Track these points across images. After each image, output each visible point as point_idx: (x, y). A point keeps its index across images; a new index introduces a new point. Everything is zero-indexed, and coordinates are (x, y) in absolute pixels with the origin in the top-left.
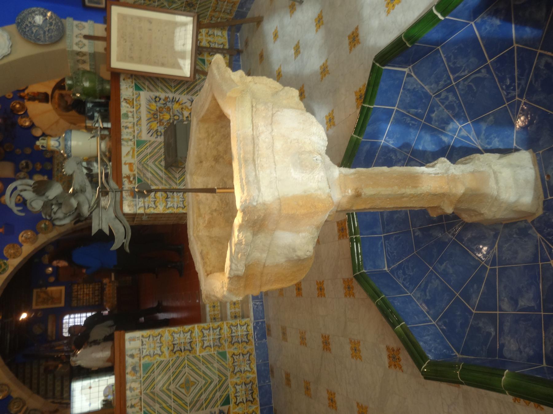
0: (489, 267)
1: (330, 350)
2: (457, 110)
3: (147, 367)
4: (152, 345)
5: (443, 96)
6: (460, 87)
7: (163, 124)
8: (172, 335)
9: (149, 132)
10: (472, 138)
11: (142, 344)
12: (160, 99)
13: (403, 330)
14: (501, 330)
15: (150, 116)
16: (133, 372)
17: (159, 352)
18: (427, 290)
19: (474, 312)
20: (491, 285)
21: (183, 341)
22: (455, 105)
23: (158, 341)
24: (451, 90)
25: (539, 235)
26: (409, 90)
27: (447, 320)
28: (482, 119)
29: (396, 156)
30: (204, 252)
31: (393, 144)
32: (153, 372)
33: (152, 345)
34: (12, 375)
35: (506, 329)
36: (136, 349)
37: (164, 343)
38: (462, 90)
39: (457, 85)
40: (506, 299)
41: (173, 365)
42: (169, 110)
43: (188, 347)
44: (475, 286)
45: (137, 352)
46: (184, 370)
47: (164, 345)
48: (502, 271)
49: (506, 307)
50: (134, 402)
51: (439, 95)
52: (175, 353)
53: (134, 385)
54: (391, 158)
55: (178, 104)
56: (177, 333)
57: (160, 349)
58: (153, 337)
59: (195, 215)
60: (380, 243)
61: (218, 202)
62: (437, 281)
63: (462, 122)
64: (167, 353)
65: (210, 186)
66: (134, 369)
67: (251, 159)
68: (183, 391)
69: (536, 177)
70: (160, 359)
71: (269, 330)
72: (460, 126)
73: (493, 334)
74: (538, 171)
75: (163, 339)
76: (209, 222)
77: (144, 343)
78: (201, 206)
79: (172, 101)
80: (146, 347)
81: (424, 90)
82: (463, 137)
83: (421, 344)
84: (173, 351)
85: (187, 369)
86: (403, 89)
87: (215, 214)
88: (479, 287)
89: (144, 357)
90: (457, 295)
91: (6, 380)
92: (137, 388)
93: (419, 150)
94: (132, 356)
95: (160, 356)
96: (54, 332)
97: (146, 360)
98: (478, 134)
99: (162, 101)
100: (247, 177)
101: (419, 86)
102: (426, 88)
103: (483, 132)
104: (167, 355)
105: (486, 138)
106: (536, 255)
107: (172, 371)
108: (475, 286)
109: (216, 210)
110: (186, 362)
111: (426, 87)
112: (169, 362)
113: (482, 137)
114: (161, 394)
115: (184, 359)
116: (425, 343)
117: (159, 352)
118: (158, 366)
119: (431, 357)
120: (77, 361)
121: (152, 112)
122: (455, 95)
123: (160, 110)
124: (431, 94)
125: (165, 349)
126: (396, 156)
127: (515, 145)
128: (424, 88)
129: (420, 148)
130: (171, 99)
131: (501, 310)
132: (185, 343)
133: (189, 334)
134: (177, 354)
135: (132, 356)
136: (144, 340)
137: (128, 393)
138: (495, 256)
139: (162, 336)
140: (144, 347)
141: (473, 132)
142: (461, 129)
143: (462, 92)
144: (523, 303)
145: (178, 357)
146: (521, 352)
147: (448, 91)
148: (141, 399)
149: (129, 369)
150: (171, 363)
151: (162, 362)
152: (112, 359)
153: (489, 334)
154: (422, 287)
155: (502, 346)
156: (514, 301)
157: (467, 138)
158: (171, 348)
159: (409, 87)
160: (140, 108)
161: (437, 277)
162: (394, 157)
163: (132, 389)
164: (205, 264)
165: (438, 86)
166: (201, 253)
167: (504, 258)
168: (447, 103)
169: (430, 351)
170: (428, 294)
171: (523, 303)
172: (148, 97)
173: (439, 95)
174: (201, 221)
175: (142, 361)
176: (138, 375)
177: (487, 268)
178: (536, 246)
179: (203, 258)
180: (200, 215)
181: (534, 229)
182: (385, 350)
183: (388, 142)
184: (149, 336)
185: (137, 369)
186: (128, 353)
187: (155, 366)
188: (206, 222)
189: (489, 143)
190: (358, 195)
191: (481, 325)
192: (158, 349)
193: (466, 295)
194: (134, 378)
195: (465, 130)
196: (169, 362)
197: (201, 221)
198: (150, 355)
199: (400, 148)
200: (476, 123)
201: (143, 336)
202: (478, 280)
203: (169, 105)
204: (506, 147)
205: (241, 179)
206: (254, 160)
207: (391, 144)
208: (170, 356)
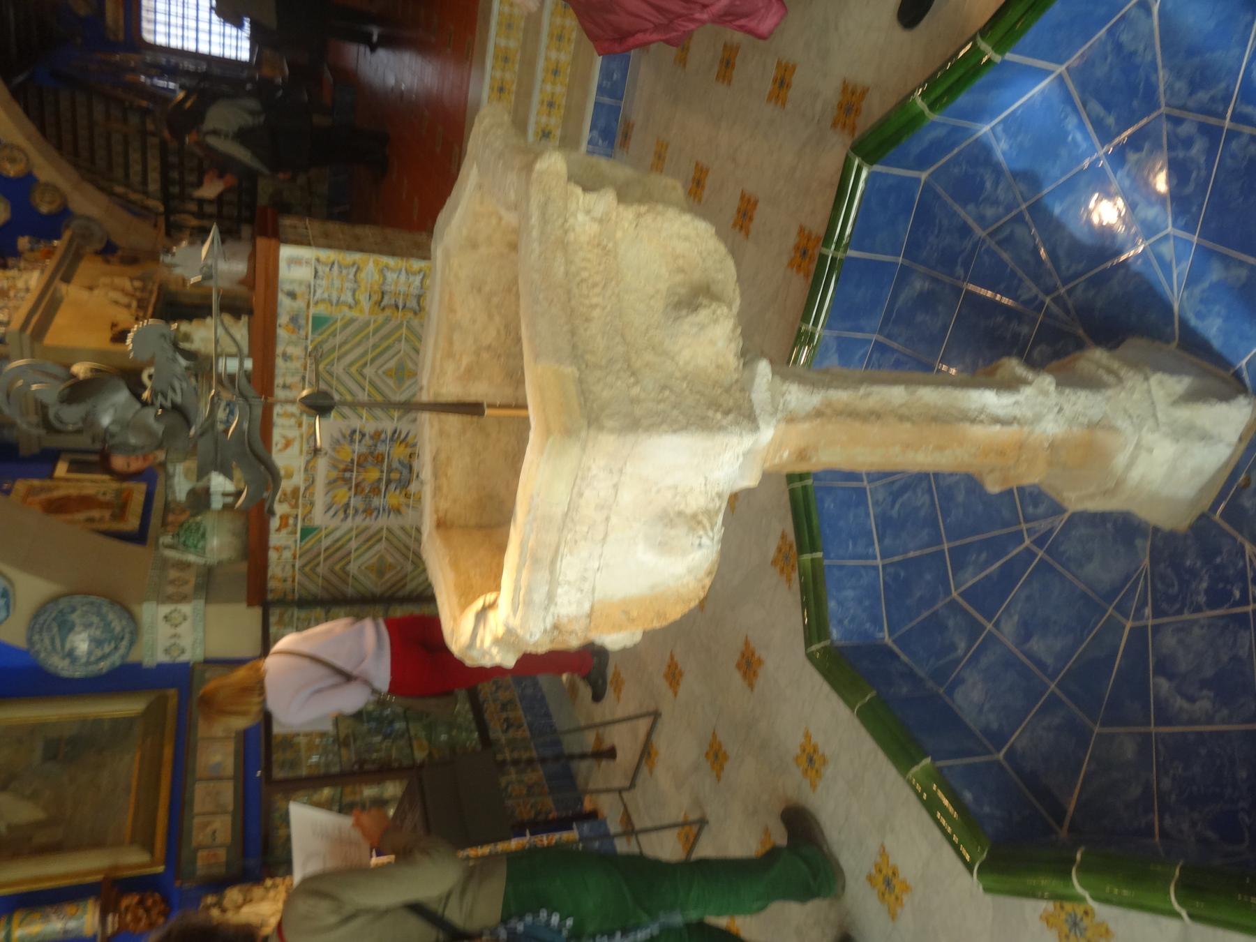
0: (1027, 542)
1: (743, 197)
2: (1189, 189)
3: (319, 322)
4: (337, 283)
5: (1186, 129)
6: (1234, 145)
7: (363, 490)
8: (381, 272)
9: (329, 509)
10: (1175, 276)
11: (316, 276)
12: (363, 435)
13: (813, 567)
14: (975, 658)
15: (334, 474)
16: (291, 326)
17: (350, 300)
18: (900, 501)
19: (954, 594)
20: (1008, 576)
21: (403, 288)
22: (1194, 175)
23: (351, 276)
24: (1211, 133)
25: (1147, 562)
26: (1119, 47)
27: (902, 574)
28: (1225, 259)
29: (996, 183)
30: (443, 456)
31: (1004, 153)
32: (334, 334)
33: (337, 283)
34: (31, 128)
35: (984, 661)
36: (301, 283)
37: (363, 285)
38: (1233, 156)
39: (1232, 135)
40: (1016, 618)
41: (376, 331)
42: (379, 460)
43: (412, 303)
44: (984, 556)
45: (303, 288)
46: (396, 345)
47: (363, 288)
48: (1043, 566)
49: (1008, 631)
50: (289, 380)
51: (1177, 121)
52: (383, 309)
53: (291, 350)
54: (982, 183)
55: (403, 445)
56: (393, 270)
57: (354, 295)
58: (340, 267)
59: (439, 356)
60: (862, 352)
61: (498, 332)
62: (926, 498)
63: (1181, 222)
64: (366, 304)
65: (472, 398)
66: (294, 319)
67: (549, 559)
68: (391, 382)
69: (1226, 464)
70: (350, 314)
71: (626, 137)
72: (1170, 229)
73: (960, 652)
74: (1236, 459)
75: (362, 275)
76: (469, 370)
77: (320, 273)
78: (456, 336)
79: (392, 439)
80: (324, 283)
81: (1153, 78)
82: (1160, 258)
83: (832, 605)
84: (379, 305)
85: (403, 345)
86: (1109, 31)
87: (485, 356)
88: (988, 563)
89: (316, 303)
90: (946, 546)
91: (18, 138)
92: (298, 358)
93: (1051, 215)
94: (292, 295)
95: (350, 307)
96: (121, 23)
97: (322, 310)
98: (1193, 279)
99: (367, 439)
100: (530, 590)
101: (1149, 58)
102: (1162, 76)
103: (1206, 285)
104: (367, 309)
105: (1202, 301)
106: (1115, 591)
107: (371, 341)
108: (984, 556)
109: (489, 347)
110: (404, 330)
111: (1161, 73)
112: (367, 324)
113: (1197, 290)
114: (345, 378)
115: (400, 326)
116: (840, 603)
117: (350, 300)
118: (345, 327)
119: (835, 633)
120: (175, 266)
121: (342, 466)
122: (1211, 152)
123: (361, 463)
124: (1163, 101)
125: (363, 298)
126: (996, 183)
127: (1244, 362)
128: (1156, 70)
129: (1057, 210)
130: (389, 433)
131: (997, 625)
132: (406, 296)
133: (418, 278)
134: (388, 312)
135: (292, 295)
136: (320, 268)
137: (279, 362)
138: (1051, 531)
139: (358, 269)
140: (319, 282)
141: (1186, 265)
142: (1166, 237)
143: (1229, 162)
144: (1037, 645)
145: (387, 320)
146: (981, 711)
147: (1204, 129)
148: (304, 378)
149: (283, 319)
150: (372, 328)
151: (352, 321)
152: (249, 281)
153: (953, 647)
154: (896, 487)
155: (960, 681)
156: (1026, 632)
157: (1166, 267)
158: (376, 297)
159: (1125, 38)
160: (310, 512)
161: (930, 490)
162: (988, 185)
163: (286, 357)
164: (437, 490)
165: (1191, 94)
166: (434, 459)
167: (1062, 548)
168: (1181, 154)
169: (840, 622)
170: (897, 507)
171: (1037, 645)
172: (337, 435)
173: (1177, 121)
174: (450, 367)
175: (312, 311)
176: (303, 333)
177: (1023, 541)
178: (1127, 578)
179: (436, 476)
180: (450, 355)
181: (1149, 543)
182: (779, 534)
183: (998, 140)
184: (333, 264)
185: (302, 321)
186: (284, 286)
187: (339, 324)
188: (462, 369)
189: (1199, 315)
190: (802, 455)
191: (951, 623)
192: (349, 294)
193: (960, 558)
194: (294, 337)
195: (1175, 247)
196: (367, 324)
197: (450, 367)
198: (331, 302)
199: (1015, 175)
200: (1204, 254)
201: (318, 260)
202: (995, 548)
203: (382, 448)
204: (1225, 352)
205: (516, 589)
206: (553, 562)
207: (1001, 149)
208: (371, 313)
